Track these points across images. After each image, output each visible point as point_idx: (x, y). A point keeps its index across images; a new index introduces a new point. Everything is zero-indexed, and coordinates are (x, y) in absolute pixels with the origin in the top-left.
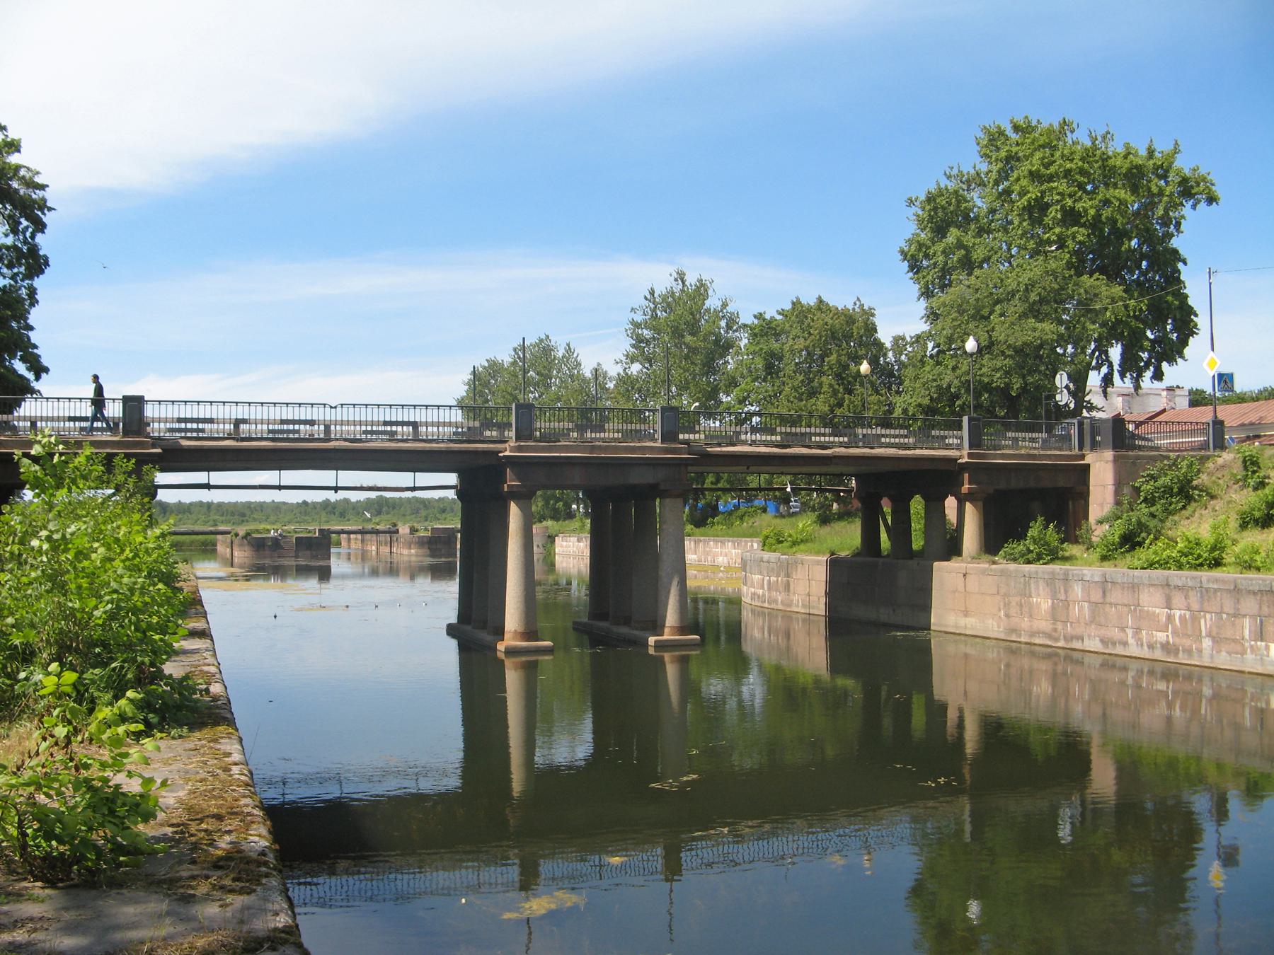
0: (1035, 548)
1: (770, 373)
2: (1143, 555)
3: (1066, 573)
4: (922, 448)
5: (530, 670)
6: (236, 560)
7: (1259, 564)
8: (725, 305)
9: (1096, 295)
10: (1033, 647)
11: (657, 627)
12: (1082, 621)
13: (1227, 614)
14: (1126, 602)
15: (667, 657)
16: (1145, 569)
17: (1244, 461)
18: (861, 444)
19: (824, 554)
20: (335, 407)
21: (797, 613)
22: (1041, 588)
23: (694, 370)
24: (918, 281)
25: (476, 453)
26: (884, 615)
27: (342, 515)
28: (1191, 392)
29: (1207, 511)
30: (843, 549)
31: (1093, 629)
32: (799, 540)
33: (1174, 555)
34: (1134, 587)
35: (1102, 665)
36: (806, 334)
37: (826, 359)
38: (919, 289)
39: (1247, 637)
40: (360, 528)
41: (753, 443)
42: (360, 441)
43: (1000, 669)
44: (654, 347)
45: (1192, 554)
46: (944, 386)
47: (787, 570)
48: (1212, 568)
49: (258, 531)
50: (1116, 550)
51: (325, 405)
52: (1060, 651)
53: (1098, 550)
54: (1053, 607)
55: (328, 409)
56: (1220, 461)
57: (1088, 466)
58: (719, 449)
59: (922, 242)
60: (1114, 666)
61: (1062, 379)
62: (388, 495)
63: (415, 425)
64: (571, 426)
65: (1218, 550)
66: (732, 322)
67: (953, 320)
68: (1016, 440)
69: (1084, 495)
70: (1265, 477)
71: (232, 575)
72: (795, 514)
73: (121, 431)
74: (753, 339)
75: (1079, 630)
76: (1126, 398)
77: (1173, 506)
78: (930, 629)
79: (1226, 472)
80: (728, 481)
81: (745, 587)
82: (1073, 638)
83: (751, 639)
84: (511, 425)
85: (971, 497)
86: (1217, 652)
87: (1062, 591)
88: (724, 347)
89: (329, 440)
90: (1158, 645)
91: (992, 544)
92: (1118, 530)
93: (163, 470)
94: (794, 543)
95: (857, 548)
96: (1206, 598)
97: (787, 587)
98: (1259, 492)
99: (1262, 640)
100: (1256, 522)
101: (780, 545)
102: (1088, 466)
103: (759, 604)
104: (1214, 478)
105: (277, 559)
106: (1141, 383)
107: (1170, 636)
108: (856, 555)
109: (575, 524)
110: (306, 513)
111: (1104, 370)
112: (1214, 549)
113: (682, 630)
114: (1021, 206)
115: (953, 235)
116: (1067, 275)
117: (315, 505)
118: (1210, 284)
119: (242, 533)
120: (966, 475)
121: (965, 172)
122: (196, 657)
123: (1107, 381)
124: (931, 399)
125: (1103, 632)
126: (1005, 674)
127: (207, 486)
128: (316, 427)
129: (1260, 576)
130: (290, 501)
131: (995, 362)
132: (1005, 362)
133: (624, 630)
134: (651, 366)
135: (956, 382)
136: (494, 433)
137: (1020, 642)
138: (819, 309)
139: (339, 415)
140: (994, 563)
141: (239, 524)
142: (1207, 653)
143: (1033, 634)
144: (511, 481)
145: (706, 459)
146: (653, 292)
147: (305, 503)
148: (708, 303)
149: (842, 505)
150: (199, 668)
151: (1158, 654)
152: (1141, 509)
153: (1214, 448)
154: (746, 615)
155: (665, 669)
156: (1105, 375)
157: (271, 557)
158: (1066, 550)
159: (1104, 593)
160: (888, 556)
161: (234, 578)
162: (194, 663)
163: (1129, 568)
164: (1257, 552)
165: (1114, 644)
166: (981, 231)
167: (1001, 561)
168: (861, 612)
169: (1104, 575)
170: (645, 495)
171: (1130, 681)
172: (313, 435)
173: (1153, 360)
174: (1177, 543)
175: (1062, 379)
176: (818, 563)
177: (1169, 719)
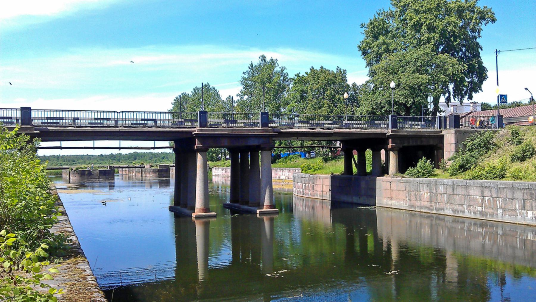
0: (422, 171)
1: (302, 99)
2: (468, 174)
3: (436, 181)
4: (371, 129)
5: (206, 225)
6: (71, 181)
7: (521, 177)
8: (282, 70)
9: (445, 63)
10: (422, 213)
11: (260, 205)
12: (443, 202)
13: (509, 199)
14: (463, 193)
15: (265, 218)
16: (471, 179)
17: (512, 133)
18: (351, 128)
19: (329, 174)
20: (120, 113)
21: (318, 199)
22: (425, 188)
23: (270, 98)
24: (366, 59)
25: (182, 132)
26: (355, 200)
27: (119, 160)
28: (482, 104)
29: (496, 154)
30: (336, 172)
31: (448, 206)
32: (317, 168)
33: (484, 173)
34: (467, 187)
35: (453, 221)
36: (317, 83)
37: (326, 93)
38: (367, 62)
39: (518, 208)
40: (128, 166)
41: (299, 128)
42: (130, 127)
43: (407, 223)
44: (253, 89)
45: (492, 173)
46: (379, 103)
47: (313, 181)
48: (501, 179)
49: (81, 168)
50: (457, 171)
51: (115, 111)
52: (434, 215)
53: (449, 171)
54: (431, 197)
55: (116, 114)
56: (501, 133)
57: (443, 135)
58: (286, 130)
59: (368, 42)
60: (458, 221)
61: (430, 99)
62: (139, 151)
63: (155, 120)
64: (223, 121)
65: (503, 171)
66: (285, 76)
67: (383, 75)
68: (412, 125)
69: (442, 148)
70: (521, 139)
71: (70, 187)
72: (313, 158)
73: (20, 123)
74: (295, 85)
75: (442, 206)
76: (455, 107)
77: (482, 152)
78: (375, 206)
79: (504, 138)
80: (285, 144)
81: (295, 188)
82: (439, 209)
83: (298, 210)
84: (197, 120)
85: (392, 149)
86: (504, 215)
87: (434, 189)
88: (282, 88)
89: (117, 127)
90: (478, 212)
91: (402, 169)
92: (458, 163)
93: (43, 141)
94: (315, 170)
95: (343, 171)
96: (499, 192)
97: (313, 188)
98: (519, 146)
99: (524, 210)
100: (518, 158)
101: (309, 171)
102: (443, 135)
103: (301, 195)
104: (499, 140)
105: (90, 180)
106: (463, 101)
107: (483, 208)
108: (343, 174)
109: (221, 163)
110: (103, 160)
111: (447, 95)
112: (501, 171)
113: (272, 206)
114: (411, 25)
115: (381, 38)
116: (433, 55)
117: (106, 156)
118: (497, 56)
119: (74, 169)
120: (390, 140)
121: (386, 11)
122: (61, 224)
123: (448, 100)
124: (373, 108)
125: (453, 206)
126: (409, 225)
127: (60, 148)
128: (110, 121)
129: (522, 182)
130: (95, 155)
131: (401, 92)
132: (406, 92)
133: (246, 207)
134: (252, 97)
135: (384, 101)
136: (190, 124)
137: (416, 211)
138: (322, 72)
139: (121, 116)
140: (403, 177)
141: (72, 165)
142: (500, 215)
143: (421, 207)
144: (198, 144)
145: (280, 135)
146: (252, 65)
147: (102, 155)
148: (275, 69)
149: (333, 154)
150: (63, 229)
151: (478, 216)
152: (467, 154)
153: (499, 128)
154: (295, 200)
155: (264, 223)
156: (447, 97)
157: (87, 179)
158: (435, 172)
159: (453, 189)
160: (356, 175)
161: (71, 188)
162: (61, 227)
163: (464, 179)
164: (521, 172)
165: (458, 212)
166: (394, 36)
167: (406, 176)
168: (345, 198)
169: (453, 182)
170: (254, 150)
171: (465, 228)
172: (109, 125)
173: (468, 91)
174: (485, 168)
175: (430, 99)
176: (326, 178)
177: (483, 245)
